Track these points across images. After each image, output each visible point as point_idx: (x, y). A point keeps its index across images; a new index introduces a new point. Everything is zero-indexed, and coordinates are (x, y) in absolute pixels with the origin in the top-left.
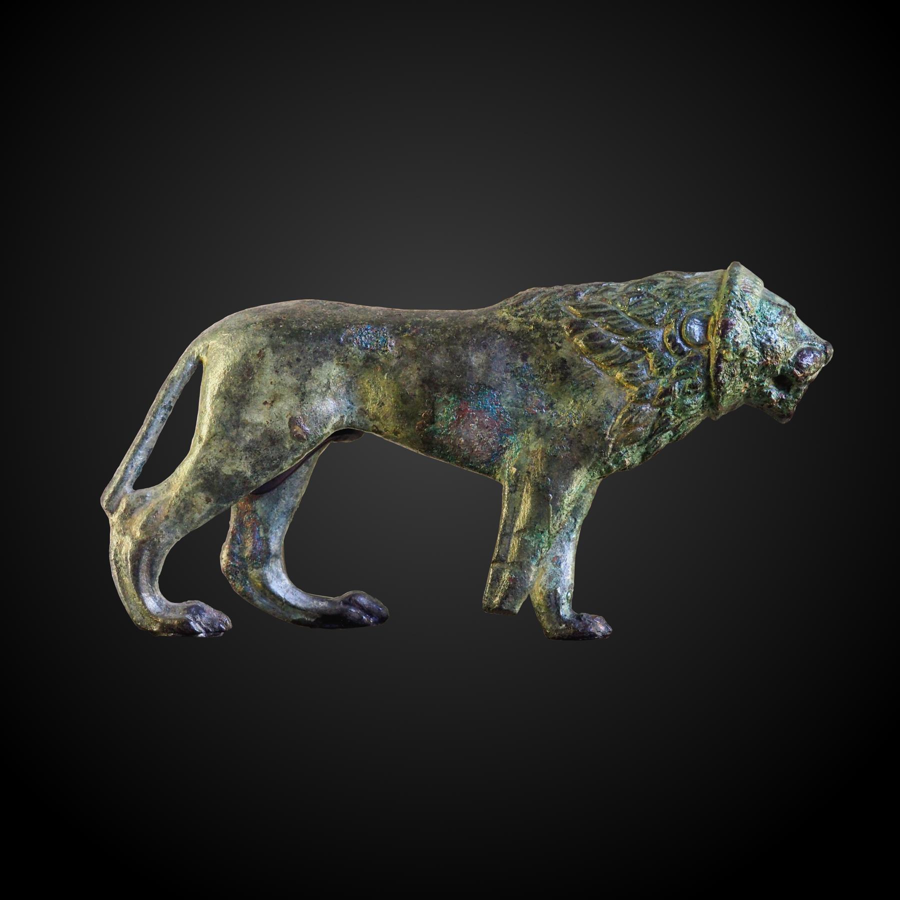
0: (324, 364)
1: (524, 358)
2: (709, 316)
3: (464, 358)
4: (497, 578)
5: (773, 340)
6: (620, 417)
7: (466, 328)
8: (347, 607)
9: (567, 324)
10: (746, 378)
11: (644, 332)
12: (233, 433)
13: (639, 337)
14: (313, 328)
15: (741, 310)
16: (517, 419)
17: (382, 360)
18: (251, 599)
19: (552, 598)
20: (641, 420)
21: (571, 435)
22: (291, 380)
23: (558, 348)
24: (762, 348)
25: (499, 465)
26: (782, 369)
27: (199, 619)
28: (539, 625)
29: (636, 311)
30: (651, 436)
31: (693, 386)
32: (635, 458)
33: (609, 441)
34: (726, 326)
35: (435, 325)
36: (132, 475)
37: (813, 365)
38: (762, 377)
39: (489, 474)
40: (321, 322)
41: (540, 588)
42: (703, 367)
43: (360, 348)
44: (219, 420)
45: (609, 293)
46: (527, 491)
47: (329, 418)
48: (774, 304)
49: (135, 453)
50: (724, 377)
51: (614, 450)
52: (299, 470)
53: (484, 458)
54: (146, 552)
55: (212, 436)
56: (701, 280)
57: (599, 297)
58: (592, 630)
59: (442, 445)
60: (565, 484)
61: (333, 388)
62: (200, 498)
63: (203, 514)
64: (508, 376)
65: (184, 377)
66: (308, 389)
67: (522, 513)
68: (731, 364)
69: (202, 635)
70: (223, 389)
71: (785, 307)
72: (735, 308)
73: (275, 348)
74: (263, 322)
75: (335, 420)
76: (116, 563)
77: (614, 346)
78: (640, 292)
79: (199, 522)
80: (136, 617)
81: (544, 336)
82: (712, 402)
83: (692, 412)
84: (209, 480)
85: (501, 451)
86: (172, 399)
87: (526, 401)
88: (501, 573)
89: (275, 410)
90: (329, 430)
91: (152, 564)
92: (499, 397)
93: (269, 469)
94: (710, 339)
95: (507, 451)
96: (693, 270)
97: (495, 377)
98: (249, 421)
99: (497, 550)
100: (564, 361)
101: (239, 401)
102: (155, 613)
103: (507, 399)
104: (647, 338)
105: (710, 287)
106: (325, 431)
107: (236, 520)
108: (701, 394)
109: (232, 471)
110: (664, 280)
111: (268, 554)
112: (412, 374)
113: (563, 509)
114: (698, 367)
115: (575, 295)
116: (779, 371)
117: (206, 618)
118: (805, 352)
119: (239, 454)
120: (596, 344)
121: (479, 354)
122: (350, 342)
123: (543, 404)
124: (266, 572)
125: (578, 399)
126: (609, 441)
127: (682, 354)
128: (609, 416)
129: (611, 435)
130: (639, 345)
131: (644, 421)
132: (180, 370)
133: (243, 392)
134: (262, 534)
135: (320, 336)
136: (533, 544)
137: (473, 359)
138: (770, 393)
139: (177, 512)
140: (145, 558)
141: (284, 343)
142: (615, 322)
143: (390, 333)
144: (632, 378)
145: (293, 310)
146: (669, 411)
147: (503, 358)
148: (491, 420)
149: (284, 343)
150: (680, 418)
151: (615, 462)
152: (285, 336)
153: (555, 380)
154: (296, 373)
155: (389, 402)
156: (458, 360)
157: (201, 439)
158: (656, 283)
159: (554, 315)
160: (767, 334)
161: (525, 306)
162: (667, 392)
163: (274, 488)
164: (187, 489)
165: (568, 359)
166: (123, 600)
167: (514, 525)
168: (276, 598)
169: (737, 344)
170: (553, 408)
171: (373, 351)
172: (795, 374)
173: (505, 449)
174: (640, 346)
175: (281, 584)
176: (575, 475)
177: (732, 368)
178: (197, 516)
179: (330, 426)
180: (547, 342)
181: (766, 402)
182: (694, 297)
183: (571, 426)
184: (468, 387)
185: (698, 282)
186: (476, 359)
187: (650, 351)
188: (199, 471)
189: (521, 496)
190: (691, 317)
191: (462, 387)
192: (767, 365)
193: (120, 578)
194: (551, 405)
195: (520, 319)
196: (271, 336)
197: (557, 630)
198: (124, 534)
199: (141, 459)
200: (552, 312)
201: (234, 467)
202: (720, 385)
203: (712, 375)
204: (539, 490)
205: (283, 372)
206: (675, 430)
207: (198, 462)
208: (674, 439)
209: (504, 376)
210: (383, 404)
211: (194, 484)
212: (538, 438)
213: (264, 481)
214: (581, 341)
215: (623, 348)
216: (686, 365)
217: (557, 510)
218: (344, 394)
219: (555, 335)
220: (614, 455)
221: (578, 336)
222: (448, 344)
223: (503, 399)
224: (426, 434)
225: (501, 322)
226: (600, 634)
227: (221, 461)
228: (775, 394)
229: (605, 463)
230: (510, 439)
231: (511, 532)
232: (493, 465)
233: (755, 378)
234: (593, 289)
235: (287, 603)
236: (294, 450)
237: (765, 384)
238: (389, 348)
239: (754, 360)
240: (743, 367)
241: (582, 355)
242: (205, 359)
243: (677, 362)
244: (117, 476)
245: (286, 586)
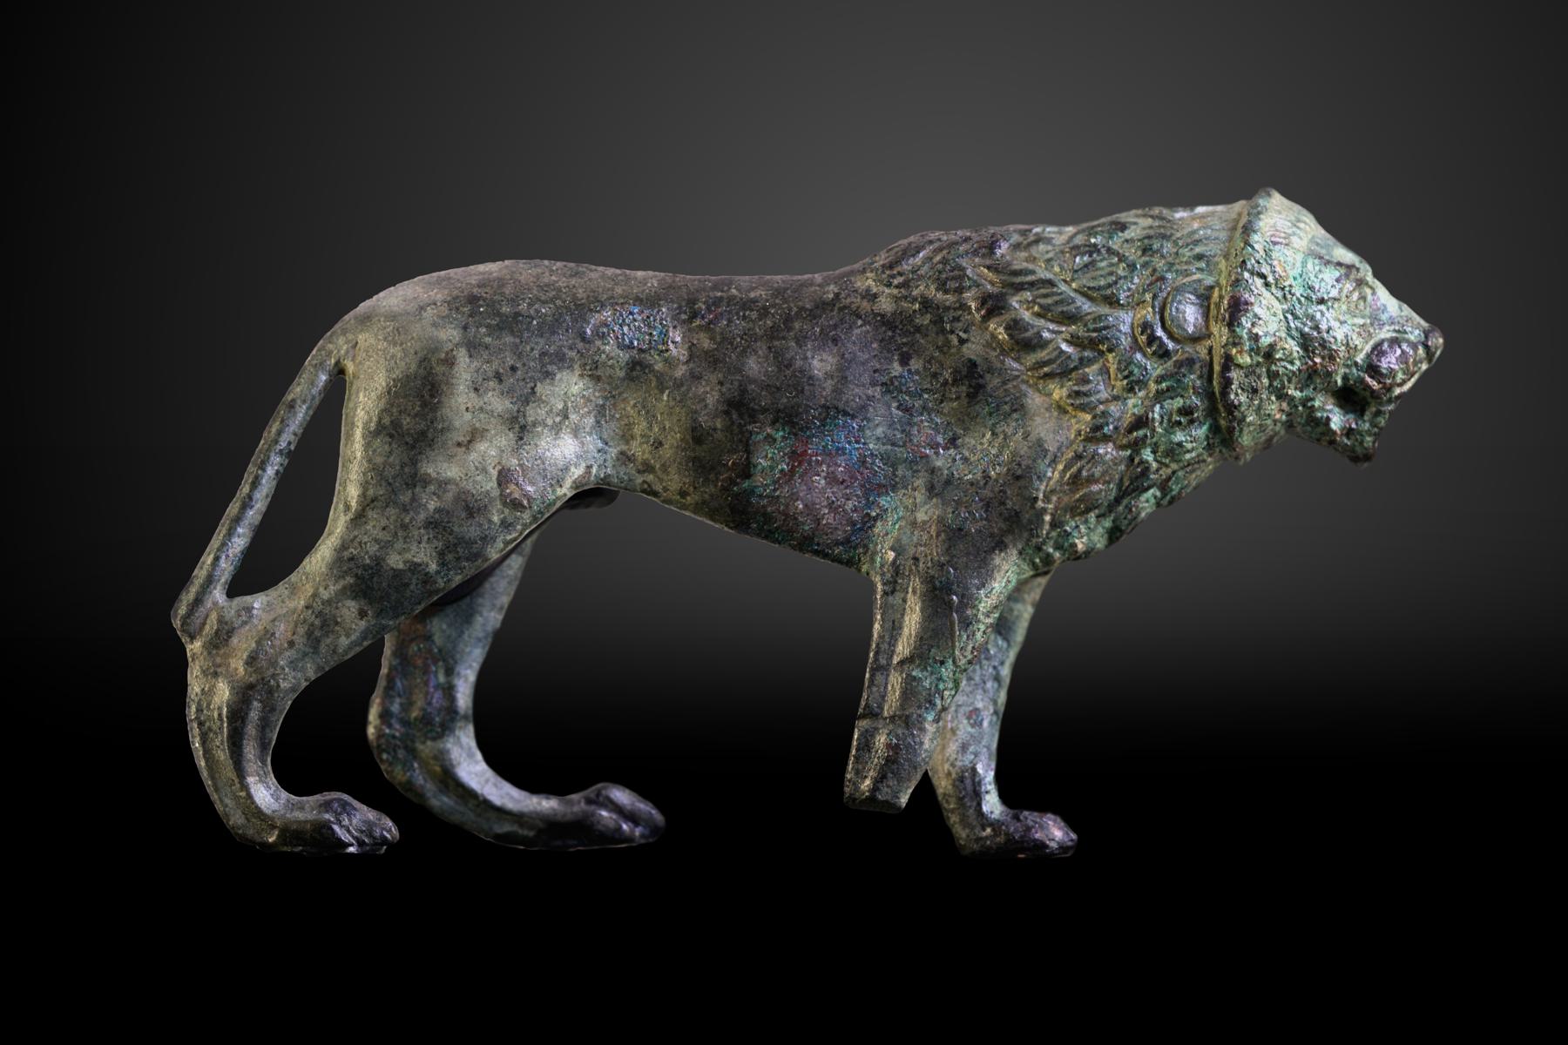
0: (558, 376)
1: (904, 361)
2: (1211, 288)
3: (799, 363)
4: (866, 746)
5: (1324, 327)
6: (1060, 467)
7: (802, 309)
8: (593, 807)
9: (975, 299)
10: (1281, 396)
11: (1099, 318)
12: (405, 497)
13: (1091, 327)
14: (537, 311)
15: (1263, 276)
16: (894, 466)
17: (659, 367)
18: (422, 796)
19: (968, 782)
20: (1097, 471)
21: (987, 493)
22: (499, 403)
23: (962, 341)
24: (1305, 342)
25: (866, 547)
26: (1345, 378)
27: (346, 822)
28: (947, 832)
29: (1086, 281)
30: (1118, 500)
31: (1186, 411)
32: (1095, 538)
33: (1044, 510)
34: (1237, 307)
35: (747, 304)
36: (226, 568)
37: (1404, 370)
38: (1308, 392)
39: (849, 563)
40: (552, 301)
41: (947, 766)
42: (1200, 377)
43: (621, 346)
44: (376, 472)
45: (1042, 247)
46: (914, 592)
47: (566, 469)
48: (1328, 263)
49: (230, 533)
50: (1239, 397)
51: (1054, 524)
52: (507, 562)
53: (840, 535)
55: (367, 503)
56: (1203, 221)
57: (1024, 254)
58: (1037, 836)
59: (765, 514)
60: (978, 577)
61: (573, 417)
62: (349, 610)
63: (353, 637)
64: (877, 391)
65: (313, 398)
66: (530, 419)
67: (906, 631)
68: (1250, 371)
69: (351, 849)
70: (387, 421)
71: (1350, 267)
72: (1252, 274)
73: (473, 347)
74: (449, 303)
75: (577, 472)
76: (201, 724)
77: (1048, 342)
78: (1095, 245)
80: (236, 819)
81: (938, 321)
82: (1223, 436)
83: (1188, 456)
84: (365, 580)
85: (868, 522)
86: (292, 438)
87: (908, 434)
88: (873, 736)
89: (473, 456)
90: (566, 491)
91: (264, 724)
92: (861, 429)
93: (468, 559)
94: (1215, 329)
95: (879, 524)
96: (1190, 204)
97: (855, 394)
98: (434, 475)
99: (865, 695)
100: (973, 365)
101: (416, 441)
102: (268, 812)
103: (877, 432)
104: (1105, 328)
105: (1216, 234)
106: (560, 492)
107: (394, 654)
108: (1201, 424)
109: (405, 562)
110: (1139, 224)
111: (451, 711)
112: (710, 394)
113: (978, 621)
114: (1192, 379)
115: (992, 247)
116: (1339, 382)
117: (357, 823)
118: (1386, 345)
119: (416, 533)
120: (1024, 342)
121: (825, 356)
122: (603, 337)
123: (940, 439)
124: (449, 746)
125: (999, 430)
126: (1044, 510)
127: (1164, 354)
128: (1042, 465)
129: (1047, 499)
130: (1091, 340)
131: (1104, 473)
132: (308, 385)
133: (423, 426)
134: (442, 679)
135: (551, 327)
136: (927, 684)
137: (815, 362)
138: (1328, 419)
139: (309, 634)
140: (254, 715)
141: (488, 340)
142: (1049, 301)
143: (673, 318)
144: (1080, 400)
145: (500, 279)
146: (1147, 455)
147: (867, 361)
148: (848, 469)
149: (488, 340)
150: (1167, 466)
151: (1058, 547)
152: (488, 326)
153: (958, 398)
154: (511, 392)
155: (673, 439)
156: (788, 366)
157: (347, 507)
158: (1123, 227)
159: (953, 285)
160: (1312, 318)
161: (905, 267)
162: (1141, 422)
163: (464, 596)
164: (325, 595)
165: (979, 361)
166: (210, 790)
167: (893, 652)
168: (466, 794)
169: (1256, 338)
170: (956, 447)
171: (641, 351)
172: (1368, 386)
173: (875, 519)
174: (1093, 344)
175: (474, 771)
176: (997, 561)
177: (1252, 378)
178: (344, 642)
179: (568, 483)
180: (943, 331)
181: (1323, 434)
182: (1187, 253)
183: (987, 477)
184: (807, 412)
185: (1196, 225)
186: (821, 364)
187: (1110, 350)
188: (343, 561)
189: (905, 601)
190: (1178, 290)
191: (799, 414)
192: (1315, 371)
193: (207, 753)
194: (953, 442)
195: (895, 291)
196: (465, 328)
197: (979, 839)
198: (216, 675)
199: (239, 543)
200: (951, 279)
201: (408, 556)
202: (1231, 408)
203: (1217, 390)
204: (935, 588)
205: (487, 390)
206: (1164, 486)
207: (344, 547)
208: (1165, 502)
209: (870, 392)
210: (661, 444)
211: (339, 587)
212: (930, 498)
213: (458, 579)
214: (1001, 330)
215: (1064, 347)
216: (1172, 376)
217: (967, 623)
218: (593, 427)
219: (957, 319)
220: (1054, 534)
221: (996, 319)
222: (772, 338)
223: (868, 433)
224: (736, 496)
225: (863, 298)
226: (1053, 845)
227: (385, 546)
228: (1337, 421)
229: (1039, 549)
230: (883, 501)
231: (889, 665)
232: (855, 548)
233: (1298, 394)
234: (1016, 238)
235: (487, 804)
236: (506, 525)
237: (1317, 404)
238: (671, 346)
239: (1292, 363)
240: (1273, 376)
241: (1003, 352)
242: (350, 367)
243: (1155, 369)
244: (200, 573)
245: (483, 773)
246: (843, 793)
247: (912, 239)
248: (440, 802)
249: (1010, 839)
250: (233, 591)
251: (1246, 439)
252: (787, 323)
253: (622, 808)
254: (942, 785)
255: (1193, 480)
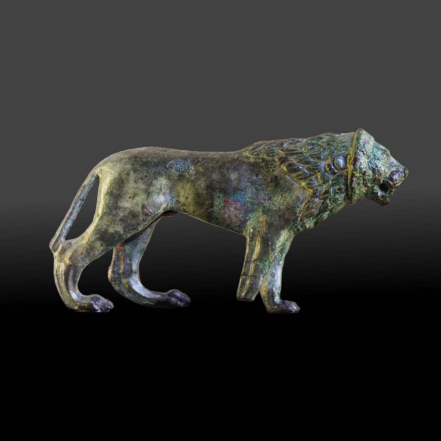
0: (159, 179)
1: (257, 175)
2: (348, 155)
3: (227, 176)
4: (243, 283)
5: (379, 167)
6: (304, 204)
7: (228, 161)
8: (170, 297)
9: (278, 159)
10: (366, 185)
11: (316, 163)
12: (114, 212)
13: (313, 165)
14: (153, 161)
15: (363, 152)
16: (253, 205)
17: (187, 176)
18: (123, 293)
19: (271, 293)
20: (314, 206)
21: (280, 213)
22: (142, 186)
23: (273, 170)
24: (374, 170)
25: (245, 228)
26: (383, 181)
27: (97, 303)
29: (312, 152)
30: (319, 214)
31: (340, 189)
32: (311, 224)
33: (299, 216)
34: (356, 160)
35: (213, 159)
36: (65, 232)
38: (373, 185)
40: (157, 158)
41: (265, 288)
42: (344, 180)
43: (177, 171)
44: (107, 206)
45: (299, 144)
46: (258, 241)
47: (161, 205)
48: (379, 149)
49: (66, 222)
50: (355, 185)
51: (301, 220)
52: (147, 230)
53: (237, 224)
54: (72, 270)
55: (104, 214)
57: (293, 146)
58: (290, 309)
59: (216, 218)
60: (277, 237)
61: (163, 190)
62: (98, 244)
63: (99, 252)
64: (249, 184)
65: (90, 185)
66: (151, 191)
67: (256, 252)
68: (358, 178)
69: (99, 311)
70: (109, 191)
71: (385, 150)
72: (360, 151)
73: (135, 170)
74: (129, 158)
75: (164, 206)
76: (57, 276)
77: (301, 169)
78: (314, 143)
79: (97, 256)
80: (67, 302)
81: (267, 165)
82: (349, 197)
83: (339, 202)
84: (103, 236)
85: (245, 221)
86: (84, 196)
87: (258, 196)
88: (246, 281)
89: (135, 201)
90: (161, 211)
91: (74, 276)
92: (244, 194)
93: (132, 230)
94: (348, 166)
95: (248, 221)
96: (339, 133)
97: (243, 185)
98: (122, 206)
99: (243, 269)
100: (276, 177)
101: (117, 196)
102: (76, 300)
103: (248, 196)
104: (317, 166)
105: (348, 140)
106: (159, 211)
107: (115, 255)
108: (343, 193)
109: (114, 231)
110: (326, 138)
111: (131, 271)
112: (202, 183)
113: (276, 249)
114: (342, 180)
115: (282, 144)
116: (382, 182)
117: (101, 303)
118: (394, 173)
119: (117, 222)
120: (292, 169)
121: (235, 174)
122: (172, 168)
123: (266, 198)
124: (130, 280)
125: (283, 196)
126: (299, 216)
127: (334, 173)
128: (298, 204)
129: (300, 213)
130: (313, 169)
131: (316, 206)
133: (119, 192)
134: (128, 262)
135: (157, 165)
136: (261, 267)
137: (232, 176)
138: (377, 193)
139: (87, 251)
140: (71, 274)
141: (139, 168)
142: (301, 158)
143: (191, 163)
144: (310, 185)
145: (144, 152)
146: (328, 201)
147: (246, 175)
148: (240, 206)
149: (139, 168)
150: (333, 205)
151: (301, 226)
152: (139, 164)
153: (272, 186)
154: (145, 183)
155: (191, 197)
156: (225, 176)
157: (98, 215)
158: (321, 139)
159: (271, 155)
160: (376, 164)
161: (257, 150)
162: (327, 192)
163: (134, 239)
164: (91, 240)
165: (278, 176)
166: (60, 294)
167: (252, 257)
168: (135, 293)
169: (361, 169)
170: (271, 200)
171: (183, 172)
172: (390, 183)
173: (248, 220)
174: (314, 170)
175: (138, 286)
176: (282, 233)
177: (359, 180)
178: (97, 253)
179: (162, 209)
180: (268, 167)
181: (375, 197)
182: (340, 145)
183: (280, 209)
184: (229, 189)
185: (342, 138)
186: (233, 176)
187: (318, 172)
188: (97, 231)
189: (255, 243)
190: (339, 155)
191: (226, 190)
192: (376, 179)
193: (59, 283)
194: (270, 199)
195: (255, 156)
196: (133, 165)
197: (273, 309)
198: (61, 262)
199: (69, 225)
200: (270, 153)
201: (115, 229)
202: (353, 189)
203: (349, 184)
204: (264, 240)
205: (139, 182)
206: (331, 211)
207: (97, 226)
208: (330, 215)
209: (247, 184)
210: (188, 198)
211: (95, 237)
212: (263, 214)
213: (129, 235)
214: (285, 167)
215: (305, 171)
216: (336, 179)
217: (273, 250)
218: (169, 193)
219: (272, 164)
220: (301, 223)
221: (283, 164)
222: (220, 169)
223: (246, 196)
224: (209, 213)
225: (245, 158)
226: (294, 311)
227: (108, 226)
228: (380, 193)
230: (250, 215)
231: (251, 261)
232: (242, 228)
233: (370, 185)
234: (291, 141)
235: (141, 296)
236: (144, 220)
237: (375, 188)
238: (191, 171)
239: (370, 176)
240: (364, 180)
241: (285, 174)
242: (100, 176)
243: (332, 177)
244: (57, 233)
245: (140, 287)
246: (236, 296)
247: (259, 142)
248: (127, 295)
249: (282, 309)
250: (67, 238)
251: (355, 198)
252: (223, 166)
253: (178, 297)
254: (263, 293)
255: (341, 207)
